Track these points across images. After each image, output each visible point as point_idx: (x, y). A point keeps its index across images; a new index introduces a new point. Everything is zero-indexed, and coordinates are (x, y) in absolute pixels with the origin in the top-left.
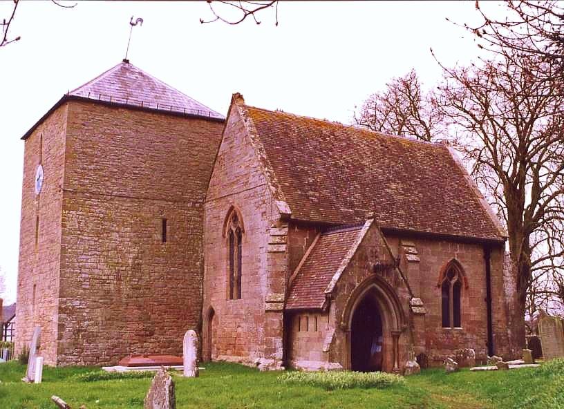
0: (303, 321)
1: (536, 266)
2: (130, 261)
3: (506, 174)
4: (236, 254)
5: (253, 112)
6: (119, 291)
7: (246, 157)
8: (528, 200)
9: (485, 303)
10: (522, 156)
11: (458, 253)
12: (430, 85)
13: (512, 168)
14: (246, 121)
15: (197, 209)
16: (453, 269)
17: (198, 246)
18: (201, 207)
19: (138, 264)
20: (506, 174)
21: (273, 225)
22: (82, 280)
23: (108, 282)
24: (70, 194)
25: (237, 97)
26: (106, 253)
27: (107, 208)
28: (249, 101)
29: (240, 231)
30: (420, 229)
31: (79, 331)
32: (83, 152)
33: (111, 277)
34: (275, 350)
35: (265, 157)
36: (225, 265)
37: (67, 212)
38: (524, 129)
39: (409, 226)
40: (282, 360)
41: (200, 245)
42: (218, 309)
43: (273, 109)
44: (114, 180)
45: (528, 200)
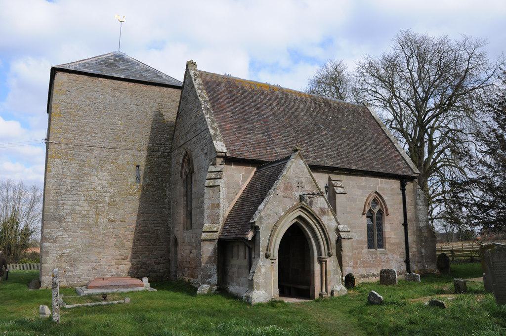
0: (235, 249)
1: (434, 199)
2: (107, 199)
3: (410, 135)
4: (189, 191)
5: (202, 74)
6: (97, 224)
7: (195, 109)
8: (426, 156)
9: (403, 227)
10: (421, 125)
11: (381, 184)
12: (351, 69)
13: (413, 132)
14: (195, 80)
15: (166, 157)
16: (377, 199)
17: (166, 186)
18: (168, 155)
19: (114, 201)
20: (410, 135)
21: (211, 163)
22: (64, 215)
23: (87, 216)
24: (56, 145)
25: (190, 64)
26: (85, 193)
27: (87, 157)
28: (201, 67)
29: (192, 172)
30: (346, 166)
31: (61, 256)
32: (69, 113)
33: (90, 213)
34: (210, 276)
35: (208, 107)
36: (182, 201)
37: (52, 159)
38: (420, 105)
39: (337, 164)
40: (217, 285)
41: (168, 186)
42: (179, 237)
43: (223, 74)
44: (93, 135)
45: (426, 156)
